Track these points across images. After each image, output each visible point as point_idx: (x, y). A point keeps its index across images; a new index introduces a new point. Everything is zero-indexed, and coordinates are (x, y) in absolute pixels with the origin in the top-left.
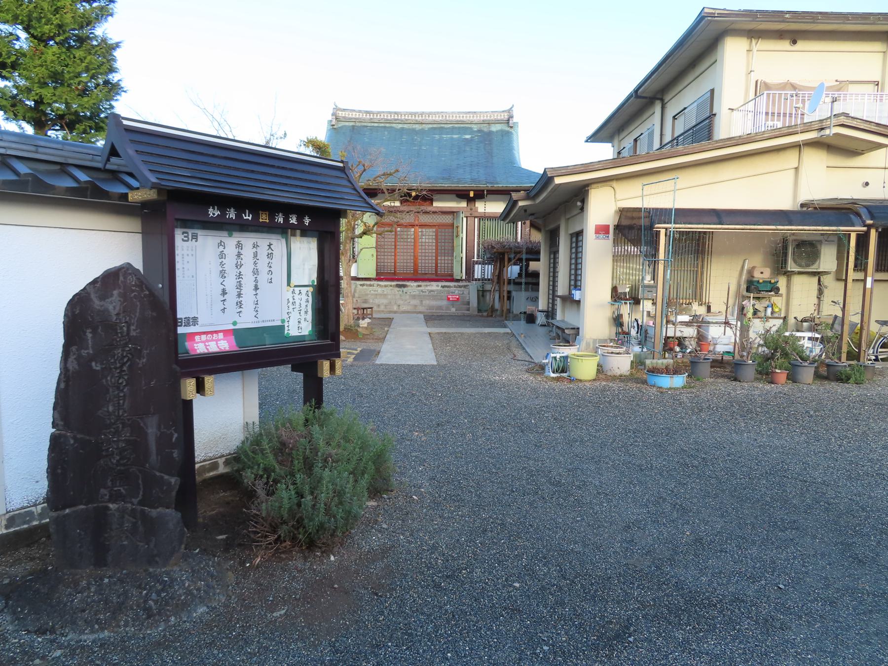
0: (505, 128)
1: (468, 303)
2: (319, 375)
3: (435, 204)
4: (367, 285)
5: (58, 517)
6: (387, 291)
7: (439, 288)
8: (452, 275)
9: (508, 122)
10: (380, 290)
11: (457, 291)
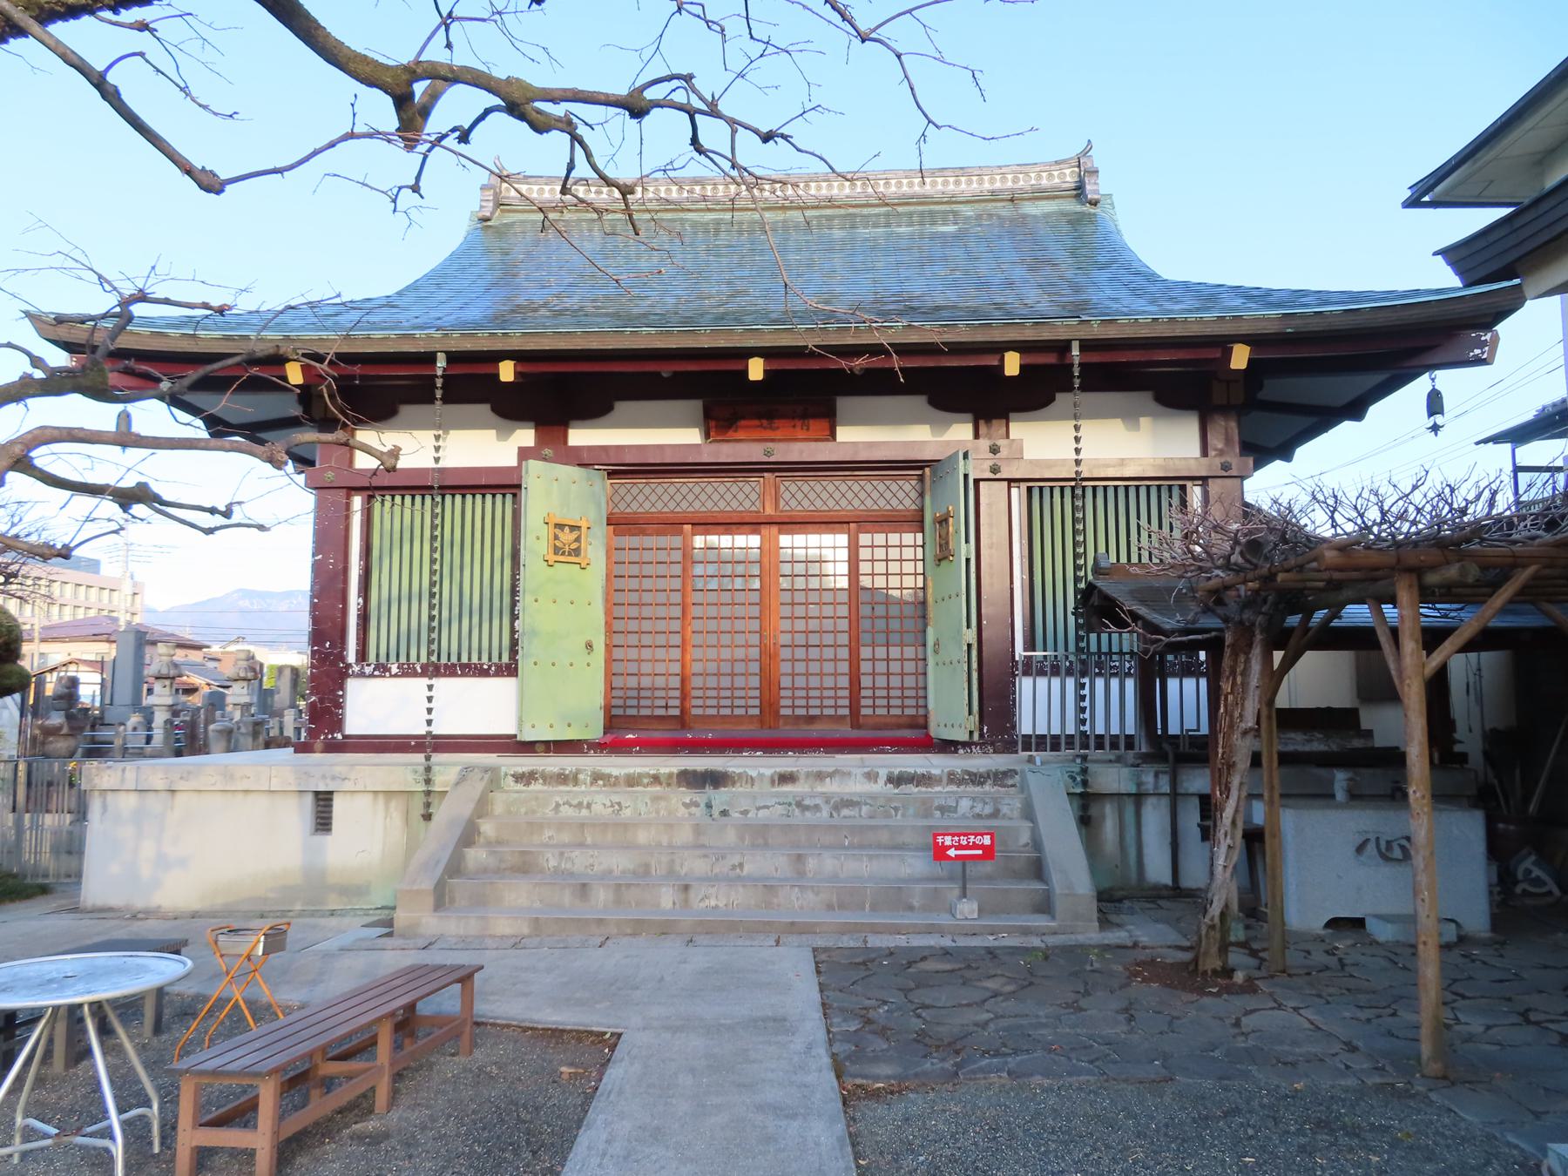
0: (1073, 206)
1: (1038, 869)
2: (1012, 415)
3: (845, 434)
4: (547, 778)
5: (112, 1158)
6: (635, 805)
7: (880, 787)
8: (921, 723)
9: (1079, 190)
10: (601, 802)
11: (966, 802)
